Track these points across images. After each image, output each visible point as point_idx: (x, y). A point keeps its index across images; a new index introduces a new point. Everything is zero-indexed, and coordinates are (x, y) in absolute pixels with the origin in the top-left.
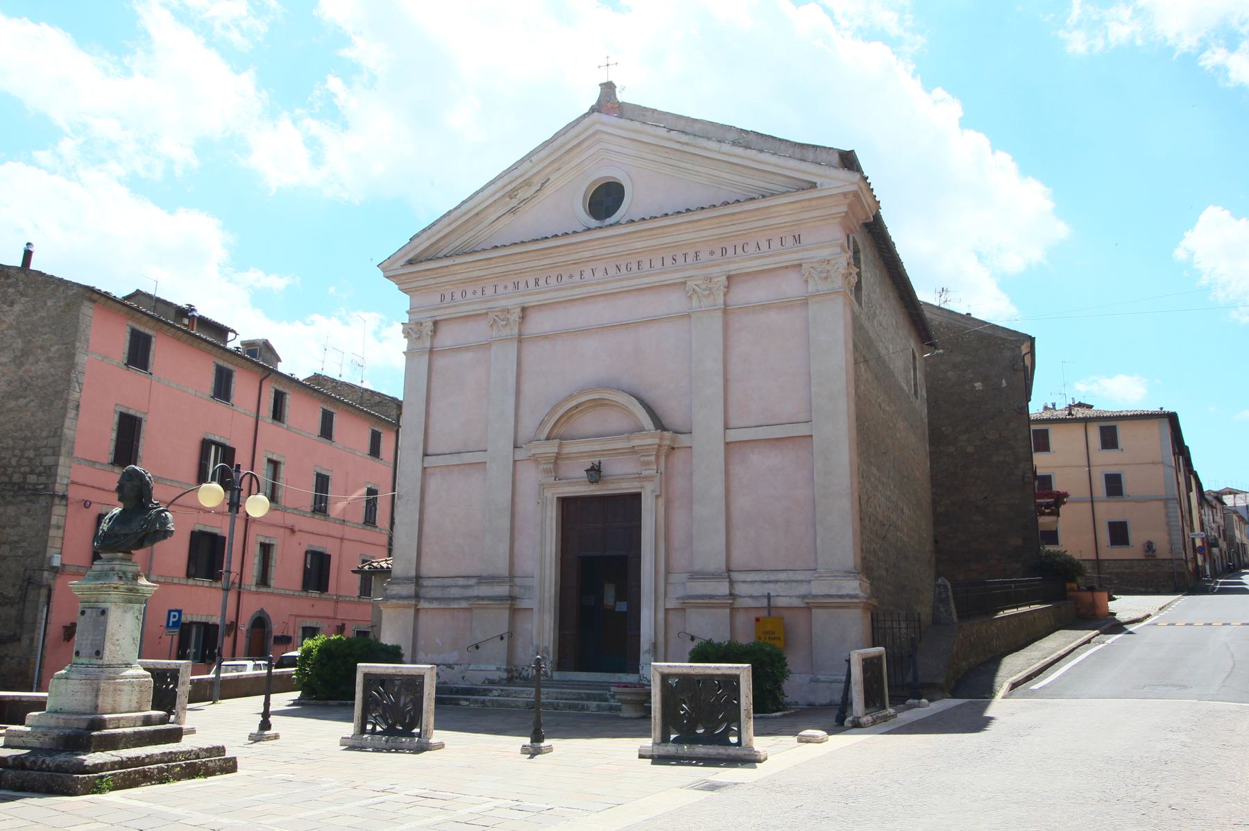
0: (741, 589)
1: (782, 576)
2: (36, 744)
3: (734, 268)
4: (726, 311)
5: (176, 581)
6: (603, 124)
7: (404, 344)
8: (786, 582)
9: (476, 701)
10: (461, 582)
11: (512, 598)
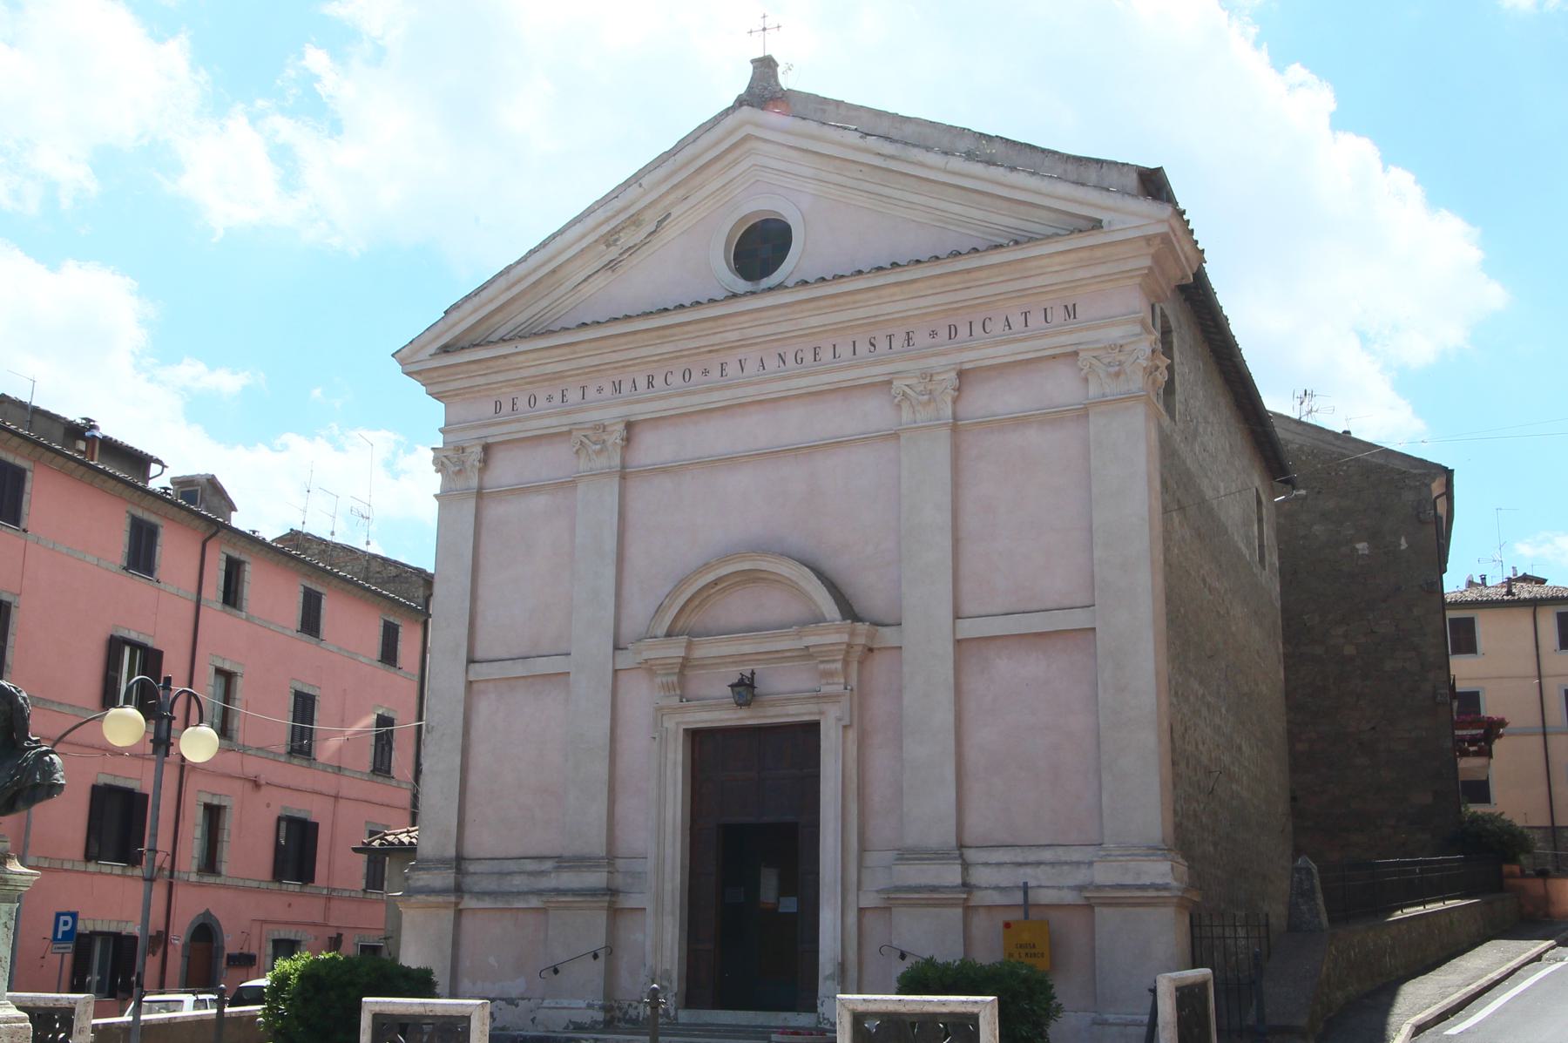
1: (1047, 855)
3: (969, 358)
4: (955, 427)
5: (67, 866)
6: (758, 125)
7: (435, 482)
8: (1053, 864)
10: (531, 866)
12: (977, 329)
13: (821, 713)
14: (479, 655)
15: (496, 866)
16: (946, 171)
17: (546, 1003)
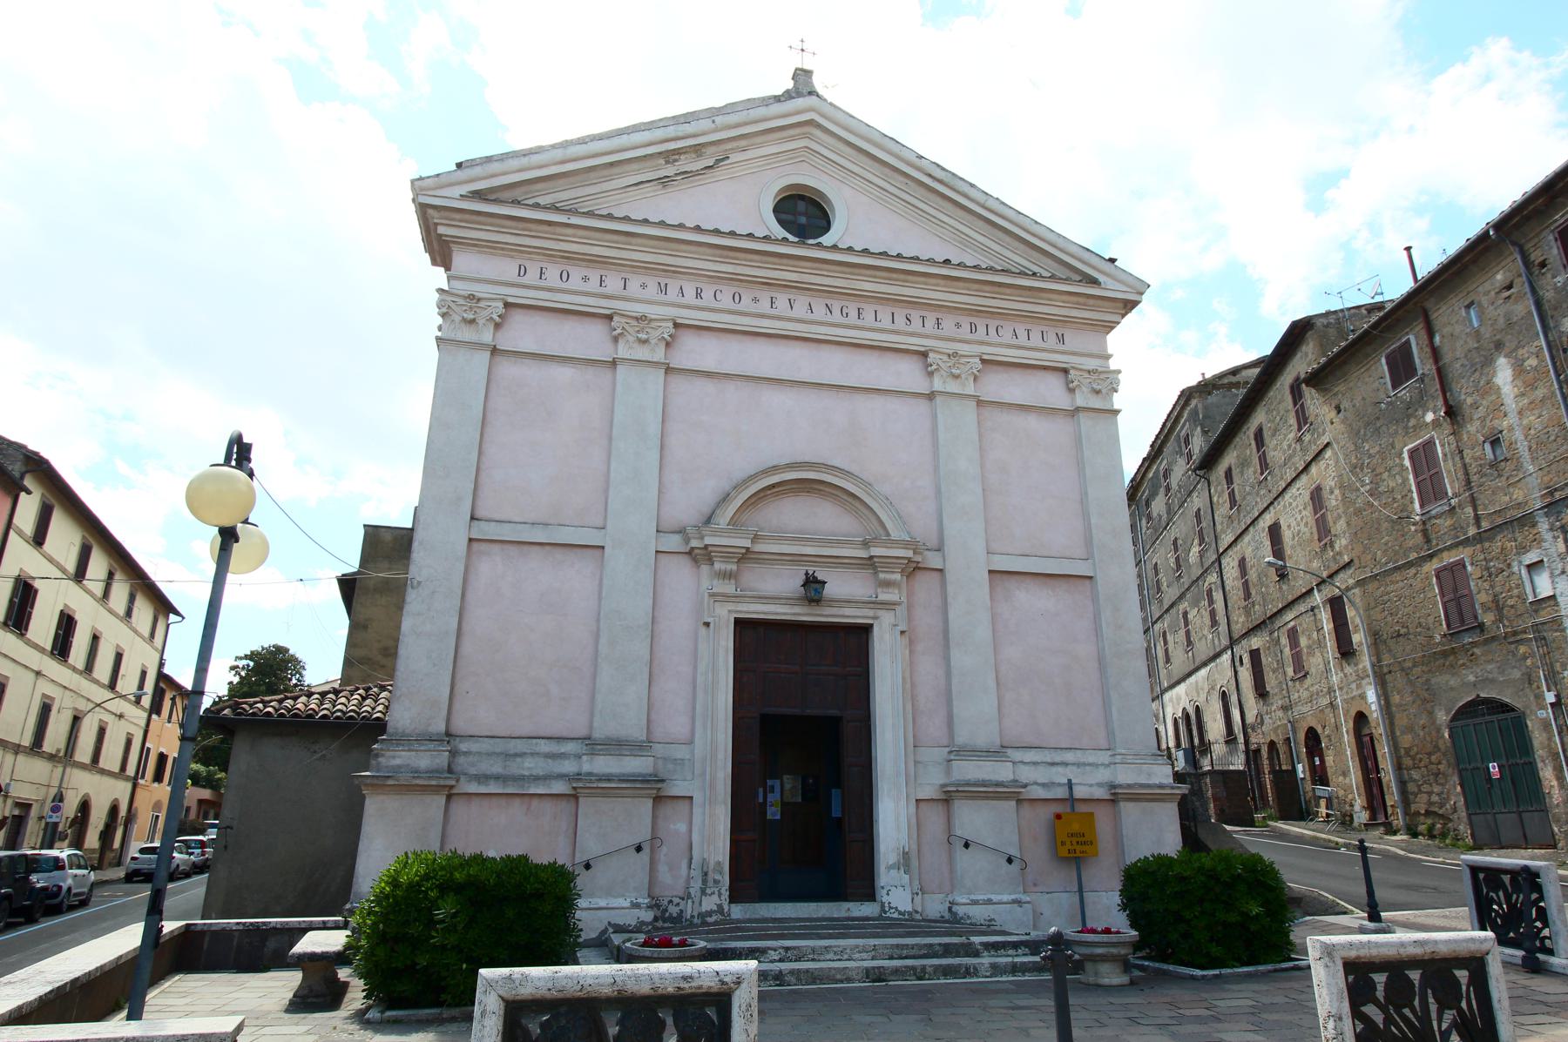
1: (1069, 757)
8: (1078, 765)
10: (545, 747)
12: (992, 331)
13: (875, 618)
14: (479, 514)
15: (499, 746)
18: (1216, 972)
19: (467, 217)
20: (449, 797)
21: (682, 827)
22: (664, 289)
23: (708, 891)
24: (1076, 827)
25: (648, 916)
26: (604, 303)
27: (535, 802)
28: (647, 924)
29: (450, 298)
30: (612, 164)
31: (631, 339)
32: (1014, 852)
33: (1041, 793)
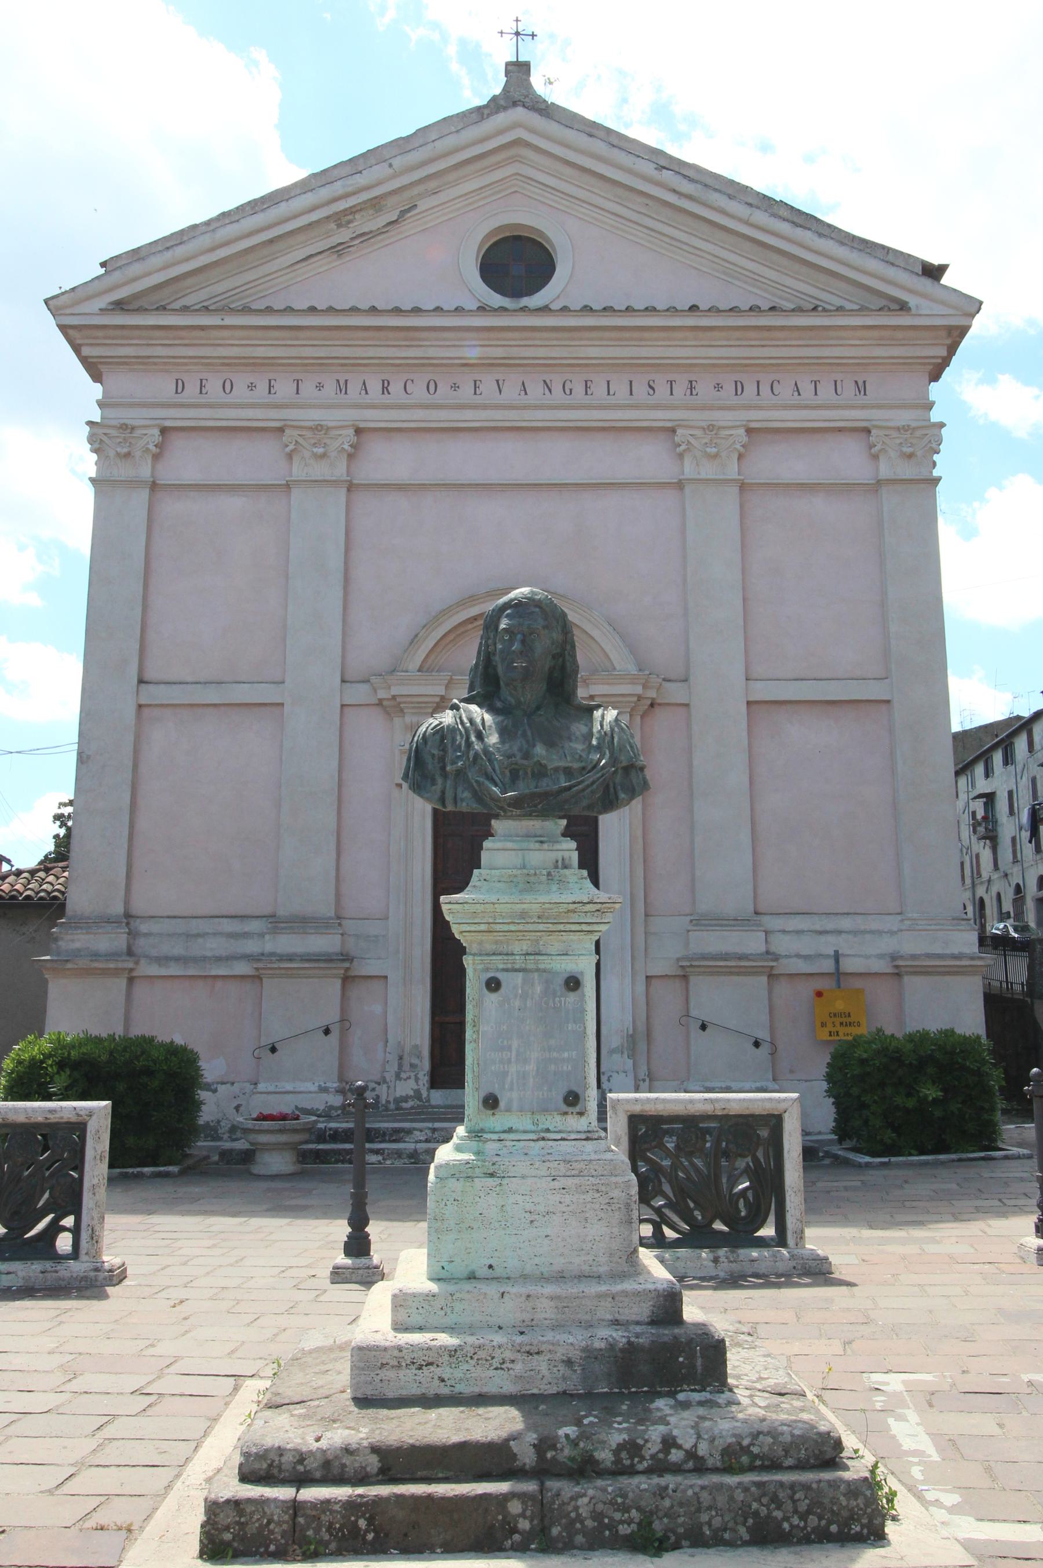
0: (783, 945)
1: (846, 923)
2: (546, 1376)
3: (757, 417)
7: (89, 463)
8: (855, 933)
9: (399, 1154)
10: (228, 926)
11: (346, 958)
12: (765, 389)
14: (149, 675)
16: (747, 223)
17: (261, 1087)
18: (886, 1160)
19: (111, 333)
20: (131, 980)
21: (378, 1009)
22: (343, 387)
23: (403, 1075)
24: (840, 1006)
25: (337, 1100)
26: (273, 414)
27: (219, 984)
28: (336, 1109)
29: (100, 431)
30: (271, 241)
31: (307, 454)
32: (763, 1035)
33: (804, 967)
